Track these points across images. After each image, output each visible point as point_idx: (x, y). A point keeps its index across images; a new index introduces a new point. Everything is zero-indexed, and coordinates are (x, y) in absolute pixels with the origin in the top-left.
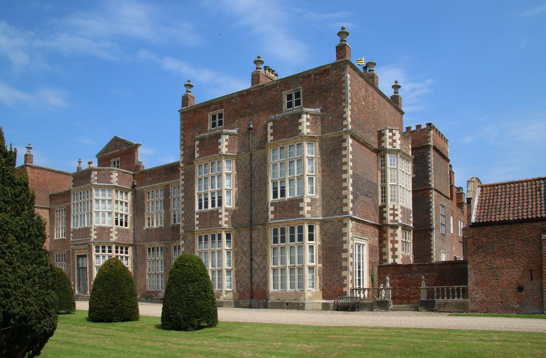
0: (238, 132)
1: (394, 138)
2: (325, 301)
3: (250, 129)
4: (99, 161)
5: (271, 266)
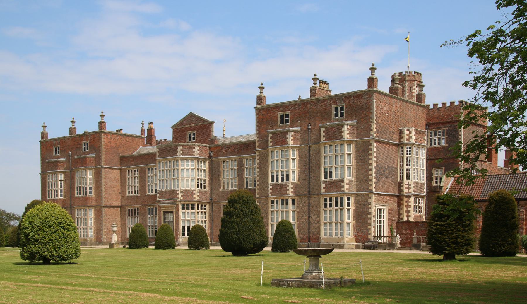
0: (300, 130)
1: (411, 135)
2: (357, 244)
3: (309, 129)
4: (174, 131)
5: (323, 221)
